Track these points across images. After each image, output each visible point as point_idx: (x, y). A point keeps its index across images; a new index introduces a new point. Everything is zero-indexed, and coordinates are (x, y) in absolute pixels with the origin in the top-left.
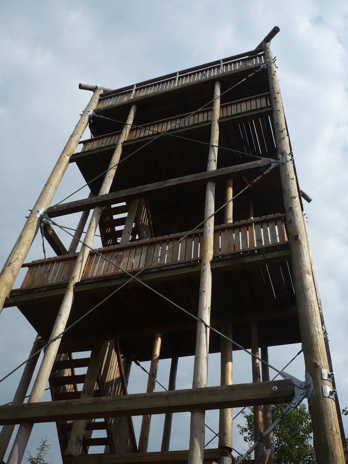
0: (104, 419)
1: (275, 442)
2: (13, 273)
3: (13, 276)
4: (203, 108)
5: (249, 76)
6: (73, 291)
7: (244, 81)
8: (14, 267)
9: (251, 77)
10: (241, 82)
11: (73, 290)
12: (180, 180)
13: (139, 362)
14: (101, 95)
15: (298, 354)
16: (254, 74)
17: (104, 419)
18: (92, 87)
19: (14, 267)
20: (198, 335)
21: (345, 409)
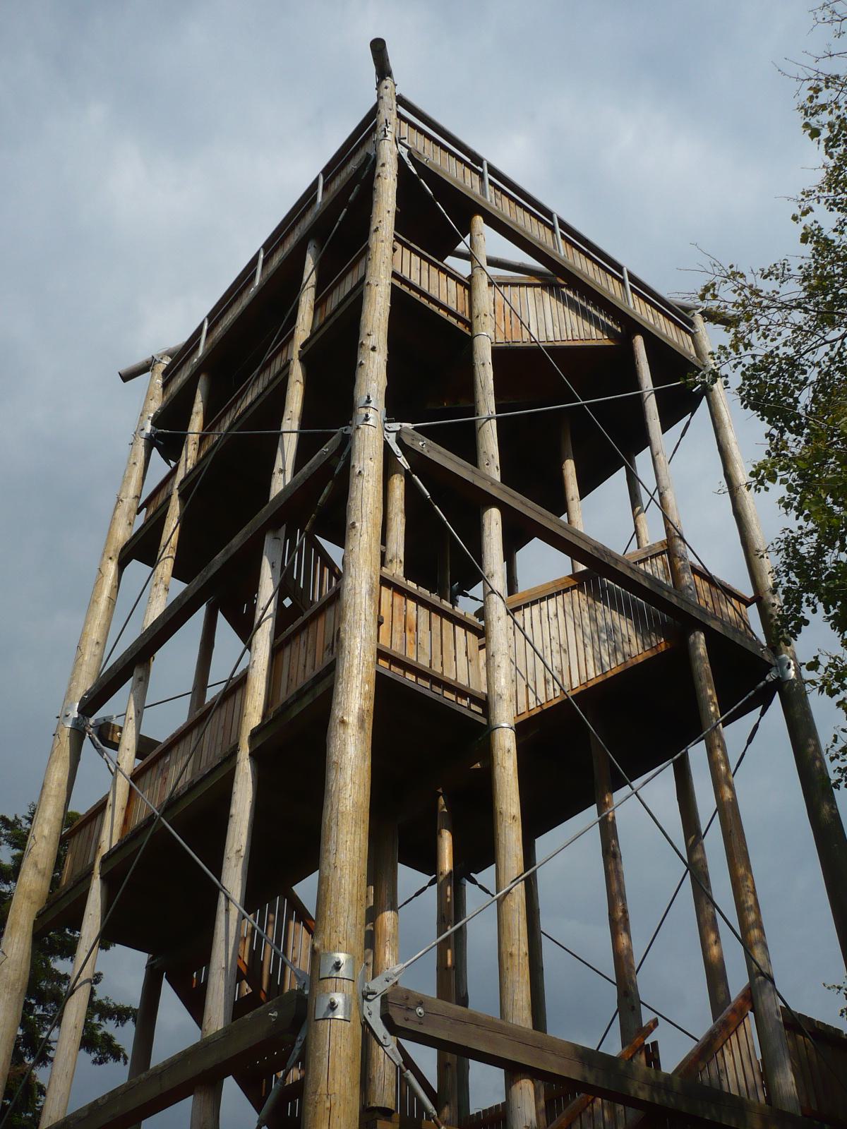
0: (293, 888)
1: (340, 943)
2: (37, 867)
3: (39, 872)
4: (275, 342)
5: (351, 198)
6: (99, 877)
7: (343, 219)
8: (38, 855)
9: (356, 197)
10: (338, 224)
11: (100, 874)
12: (227, 552)
13: (166, 977)
14: (165, 373)
15: (431, 661)
16: (359, 188)
17: (293, 888)
18: (146, 364)
19: (38, 855)
20: (250, 836)
21: (746, 367)
